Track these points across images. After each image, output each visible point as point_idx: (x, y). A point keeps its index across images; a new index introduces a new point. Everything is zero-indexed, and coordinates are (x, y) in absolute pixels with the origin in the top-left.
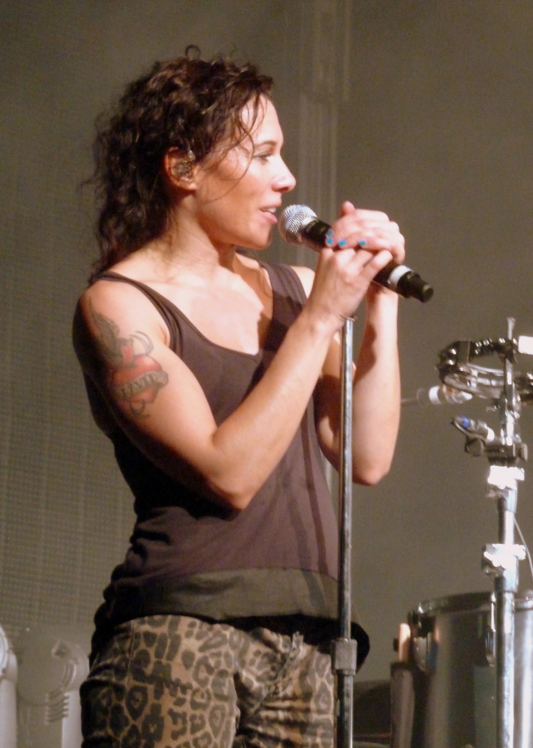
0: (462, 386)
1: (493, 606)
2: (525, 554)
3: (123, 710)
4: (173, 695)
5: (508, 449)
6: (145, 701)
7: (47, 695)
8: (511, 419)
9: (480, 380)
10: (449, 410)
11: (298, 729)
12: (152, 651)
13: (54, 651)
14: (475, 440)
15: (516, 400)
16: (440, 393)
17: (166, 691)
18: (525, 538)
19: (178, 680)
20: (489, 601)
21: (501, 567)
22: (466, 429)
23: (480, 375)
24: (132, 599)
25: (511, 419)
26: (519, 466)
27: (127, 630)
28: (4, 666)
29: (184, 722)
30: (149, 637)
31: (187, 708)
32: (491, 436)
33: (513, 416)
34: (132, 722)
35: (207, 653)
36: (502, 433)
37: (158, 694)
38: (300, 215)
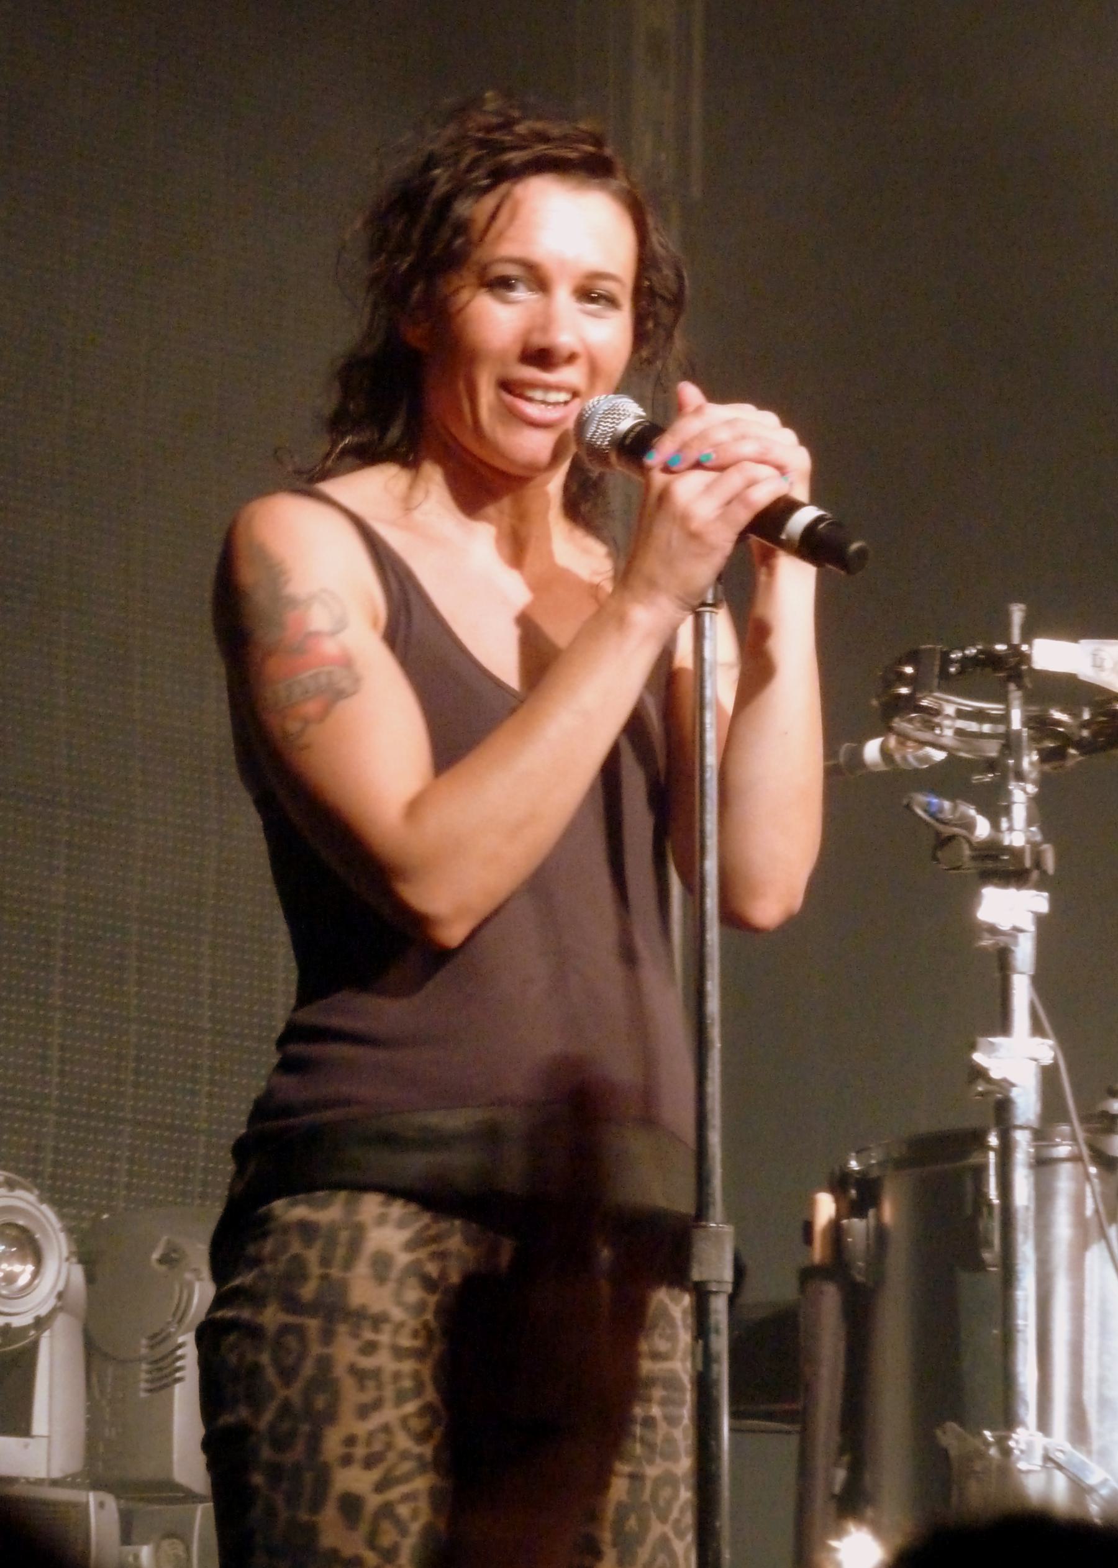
0: (927, 736)
1: (992, 1156)
2: (1052, 1054)
4: (355, 1335)
5: (1016, 853)
7: (144, 1342)
8: (1020, 796)
9: (961, 724)
10: (898, 780)
12: (312, 1256)
13: (155, 1256)
14: (952, 838)
15: (1029, 760)
16: (885, 752)
17: (342, 1329)
18: (1051, 1023)
20: (985, 1147)
21: (1005, 1080)
22: (932, 815)
23: (961, 714)
24: (284, 1156)
25: (1020, 796)
26: (1039, 887)
27: (268, 1218)
28: (60, 1287)
29: (380, 1386)
30: (307, 1230)
32: (983, 829)
33: (1024, 790)
36: (1004, 824)
37: (328, 1336)
38: (612, 412)
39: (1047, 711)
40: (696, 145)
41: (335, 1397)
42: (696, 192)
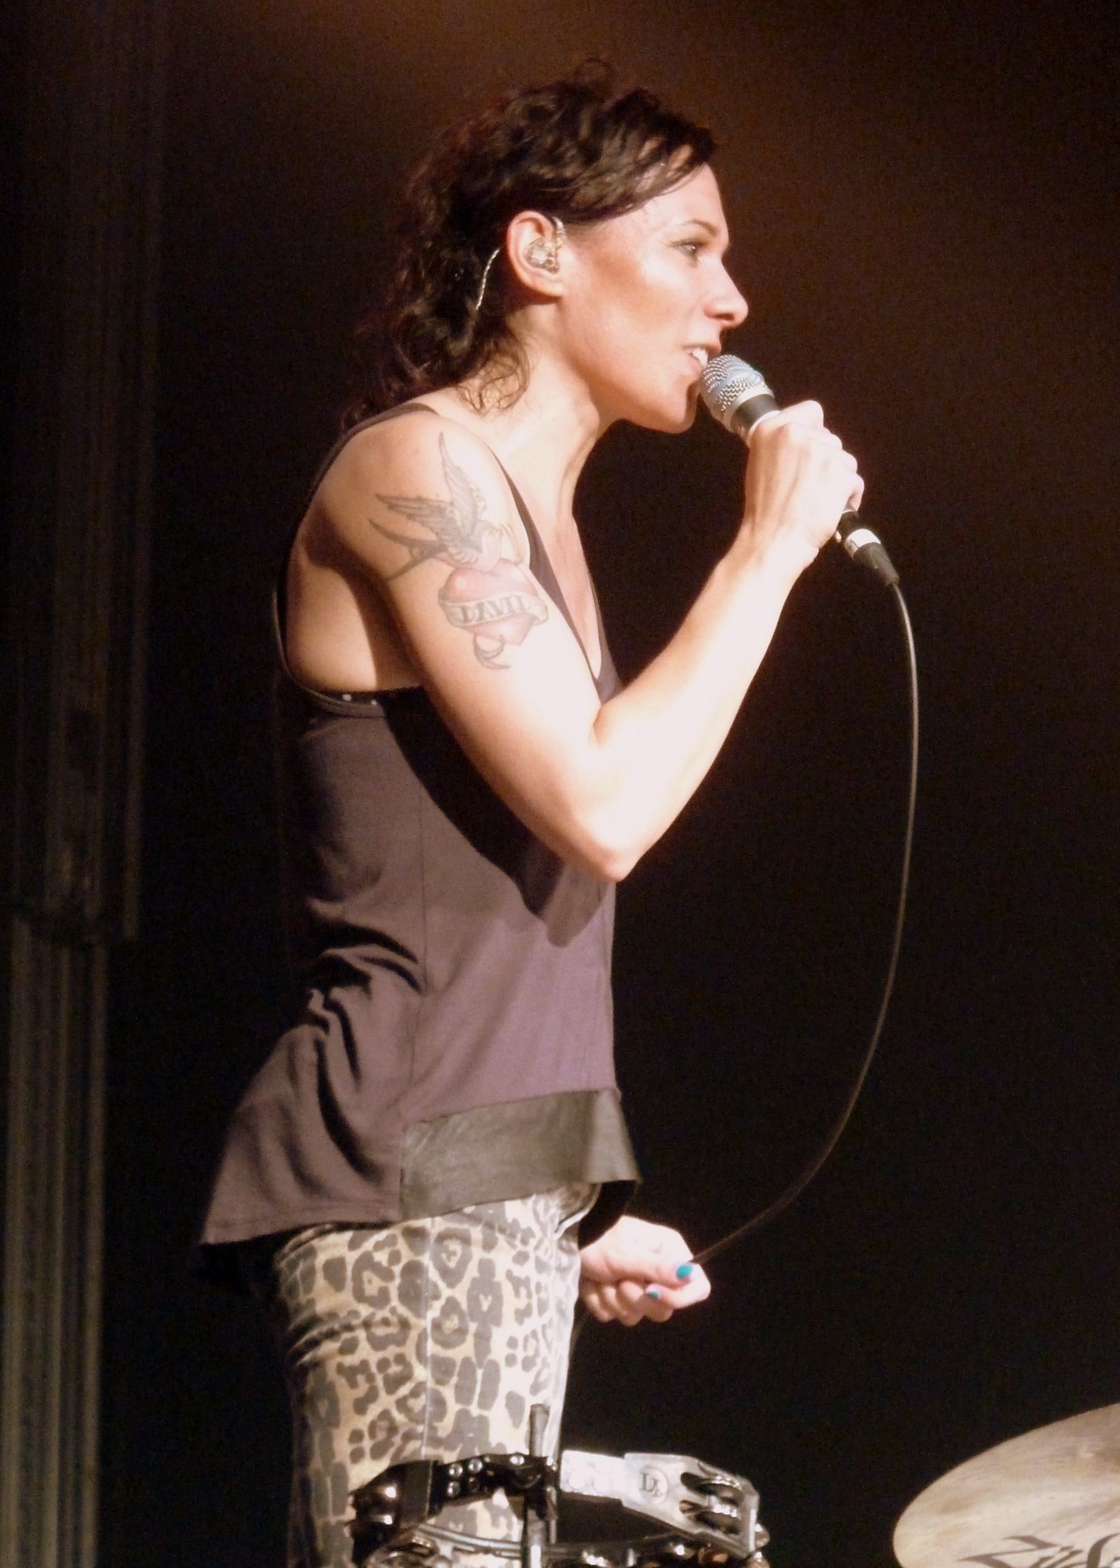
3: (427, 1272)
11: (376, 1509)
17: (501, 1239)
19: (515, 1222)
29: (370, 1378)
31: (365, 1352)
34: (446, 1292)
39: (579, 1554)
40: (131, 878)
41: (498, 1300)
42: (130, 929)
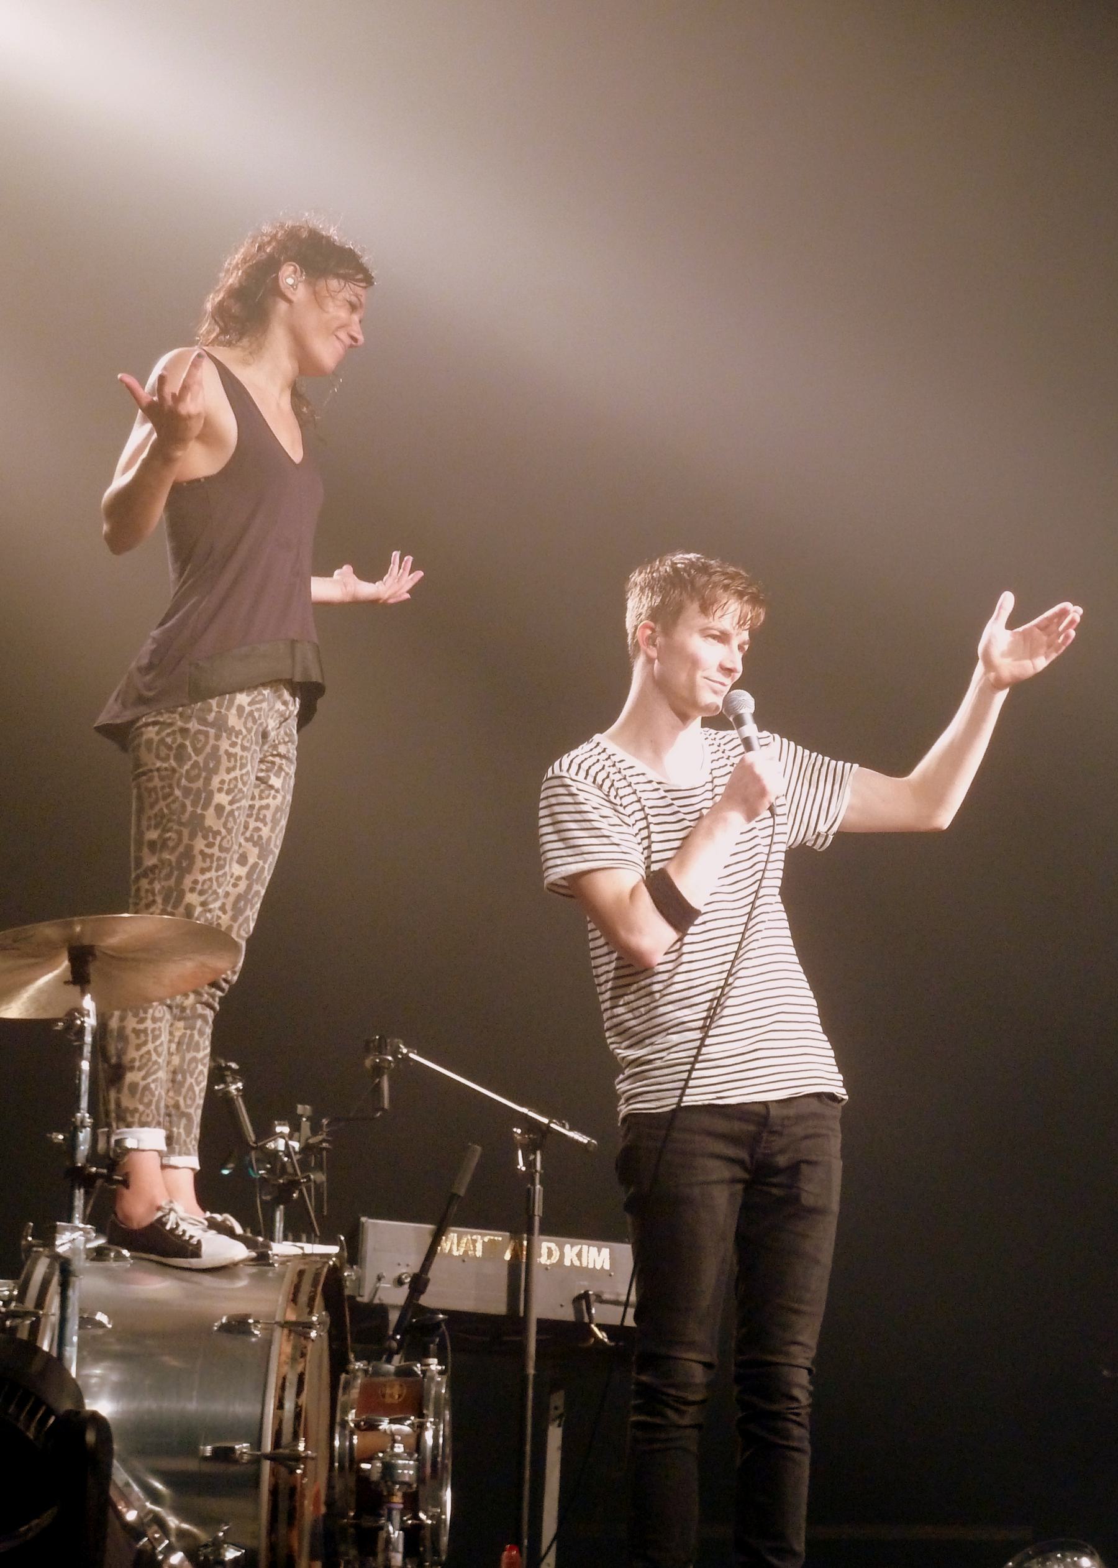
4: (229, 739)
6: (207, 743)
29: (236, 761)
31: (215, 850)
34: (194, 758)
35: (253, 708)
37: (218, 737)
